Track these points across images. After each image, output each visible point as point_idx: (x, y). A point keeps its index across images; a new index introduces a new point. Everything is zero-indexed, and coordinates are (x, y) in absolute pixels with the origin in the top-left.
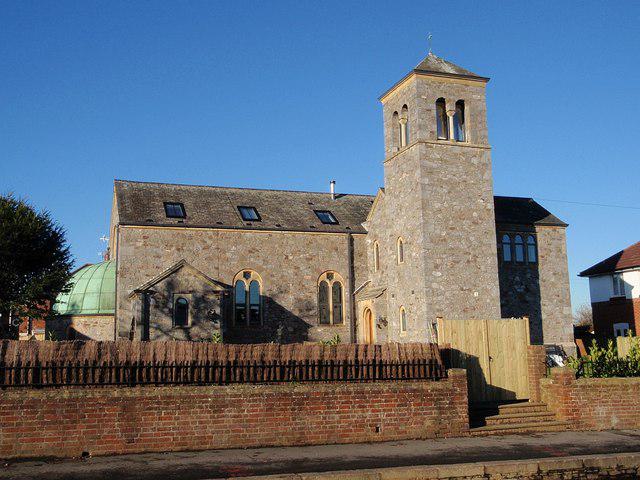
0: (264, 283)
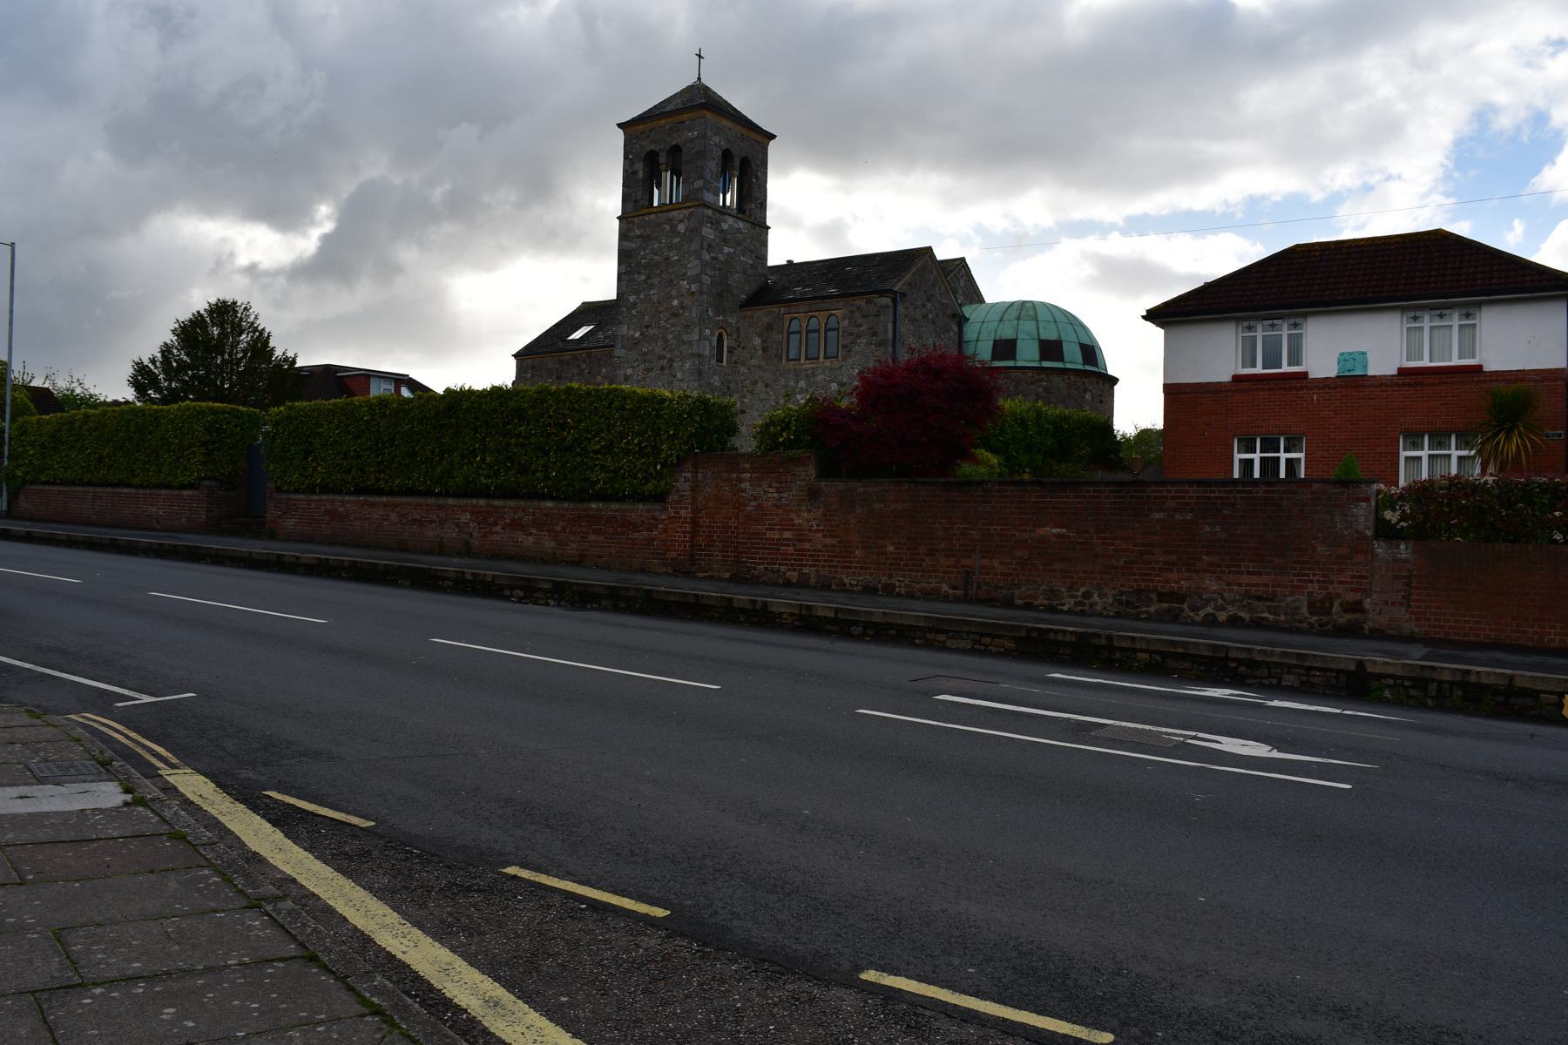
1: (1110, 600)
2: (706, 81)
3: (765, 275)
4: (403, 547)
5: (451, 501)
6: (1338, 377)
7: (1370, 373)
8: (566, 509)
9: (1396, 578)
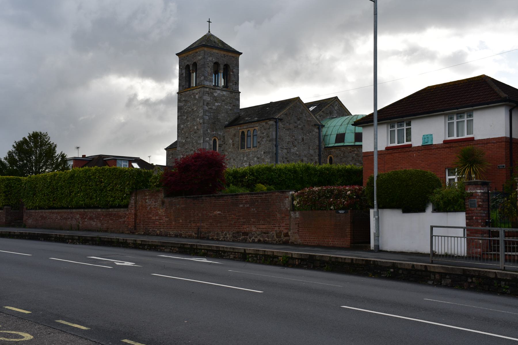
1: (231, 236)
2: (212, 32)
3: (239, 113)
5: (74, 210)
6: (422, 146)
7: (434, 143)
8: (103, 212)
9: (296, 224)
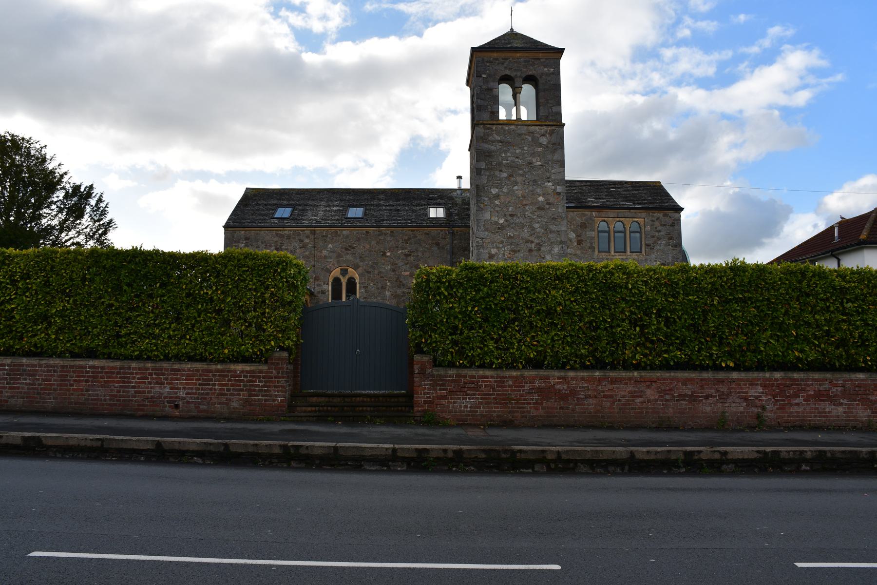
0: (361, 279)
4: (665, 425)
